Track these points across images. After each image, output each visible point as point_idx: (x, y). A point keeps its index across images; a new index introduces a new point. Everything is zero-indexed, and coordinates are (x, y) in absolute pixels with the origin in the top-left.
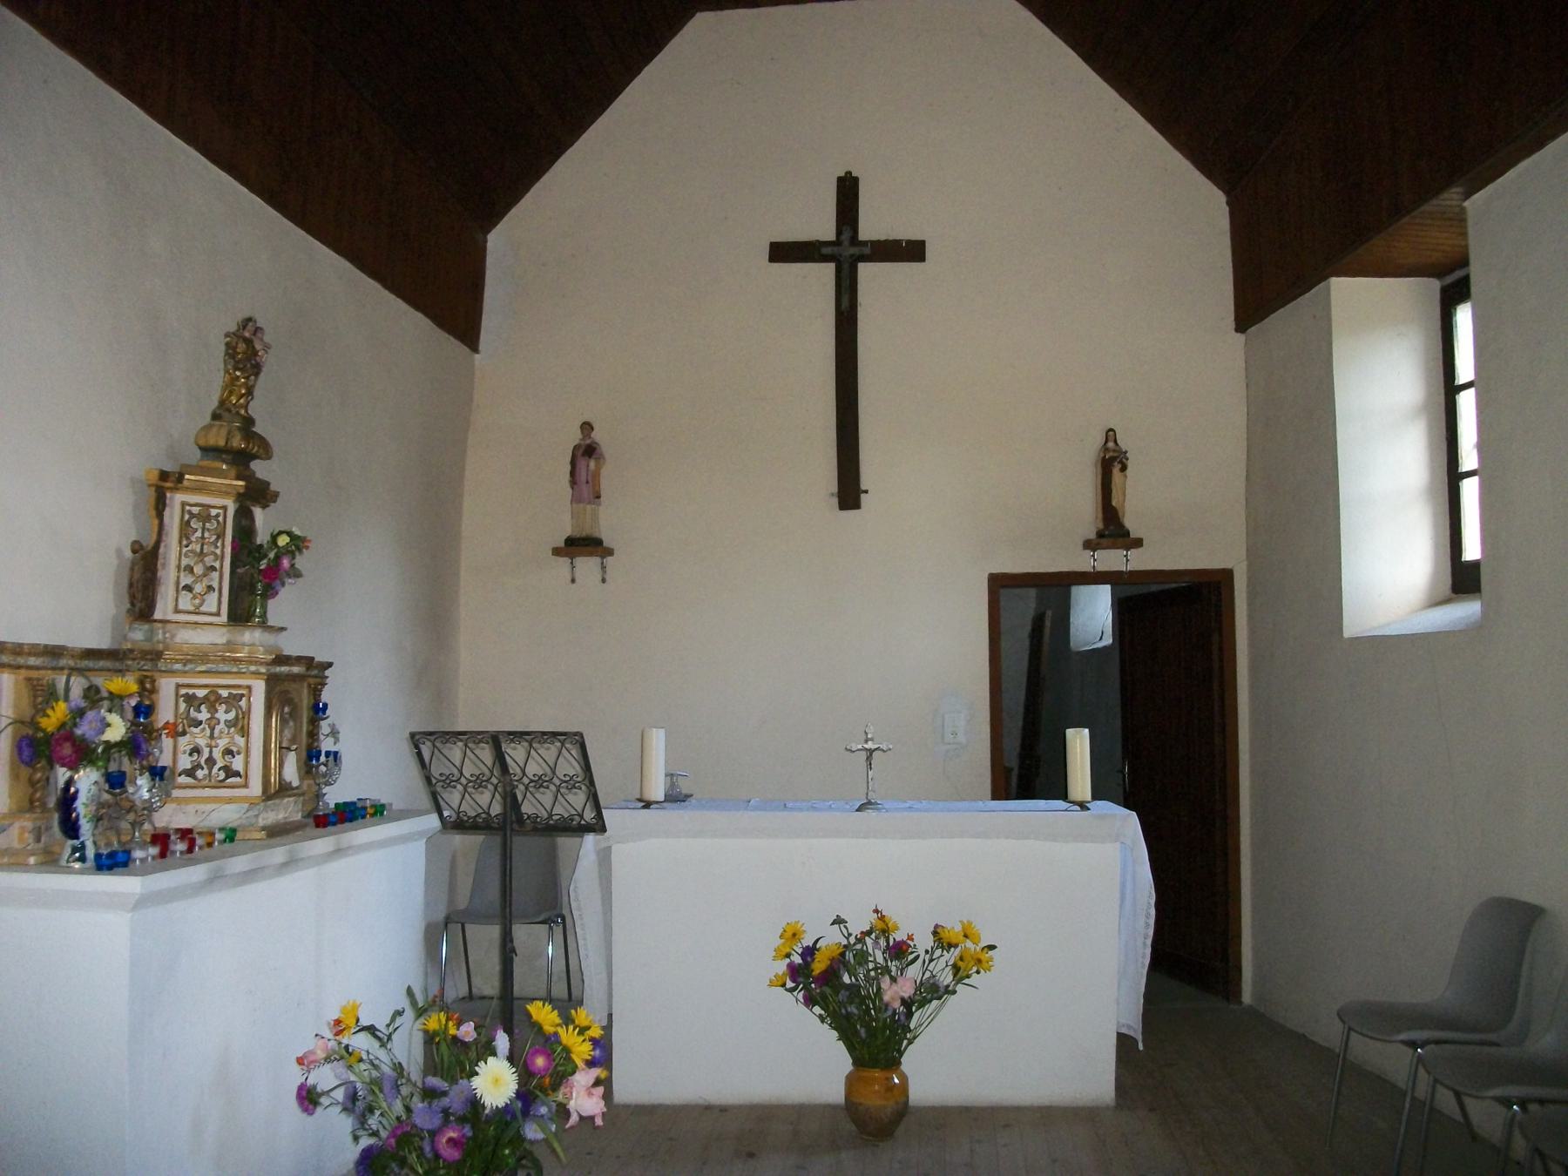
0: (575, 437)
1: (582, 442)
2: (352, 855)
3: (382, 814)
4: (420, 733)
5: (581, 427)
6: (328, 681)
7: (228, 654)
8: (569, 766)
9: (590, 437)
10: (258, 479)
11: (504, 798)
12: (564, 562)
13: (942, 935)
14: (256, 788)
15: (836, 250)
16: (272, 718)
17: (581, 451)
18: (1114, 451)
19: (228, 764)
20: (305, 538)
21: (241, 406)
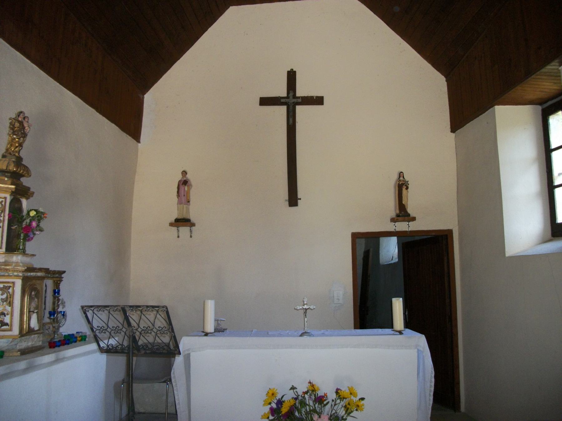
0: (179, 177)
1: (182, 179)
2: (66, 361)
3: (85, 340)
4: (86, 306)
5: (182, 173)
6: (63, 279)
7: (3, 267)
8: (160, 322)
9: (185, 177)
10: (25, 186)
11: (129, 338)
12: (174, 229)
13: (341, 394)
14: (16, 331)
15: (287, 100)
16: (25, 297)
17: (182, 183)
18: (403, 181)
19: (2, 320)
20: (44, 212)
21: (16, 152)
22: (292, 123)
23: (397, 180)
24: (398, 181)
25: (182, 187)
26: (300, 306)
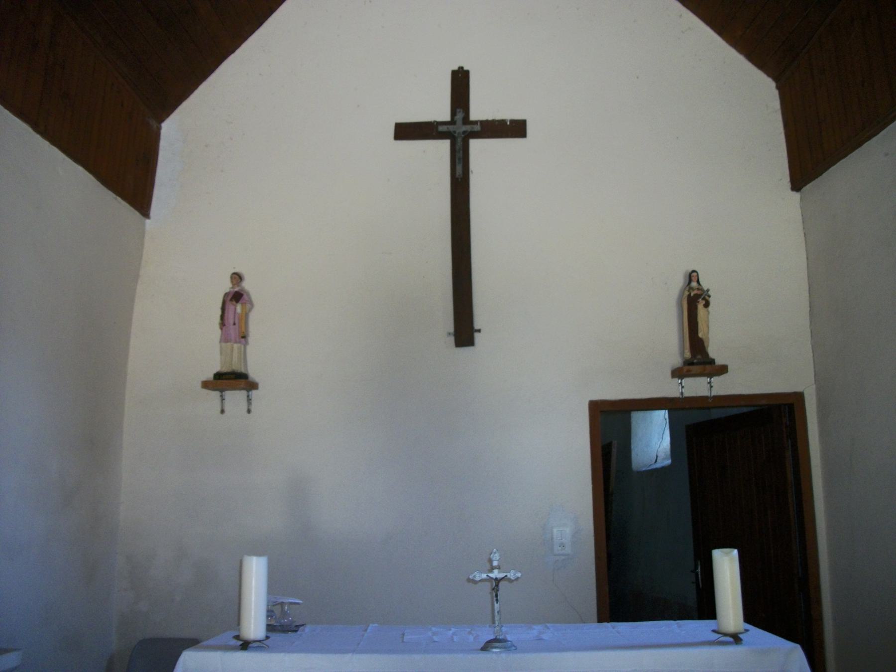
0: (227, 286)
17: (230, 297)
18: (698, 289)
22: (461, 172)
23: (685, 289)
24: (687, 289)
25: (230, 307)
26: (481, 572)
